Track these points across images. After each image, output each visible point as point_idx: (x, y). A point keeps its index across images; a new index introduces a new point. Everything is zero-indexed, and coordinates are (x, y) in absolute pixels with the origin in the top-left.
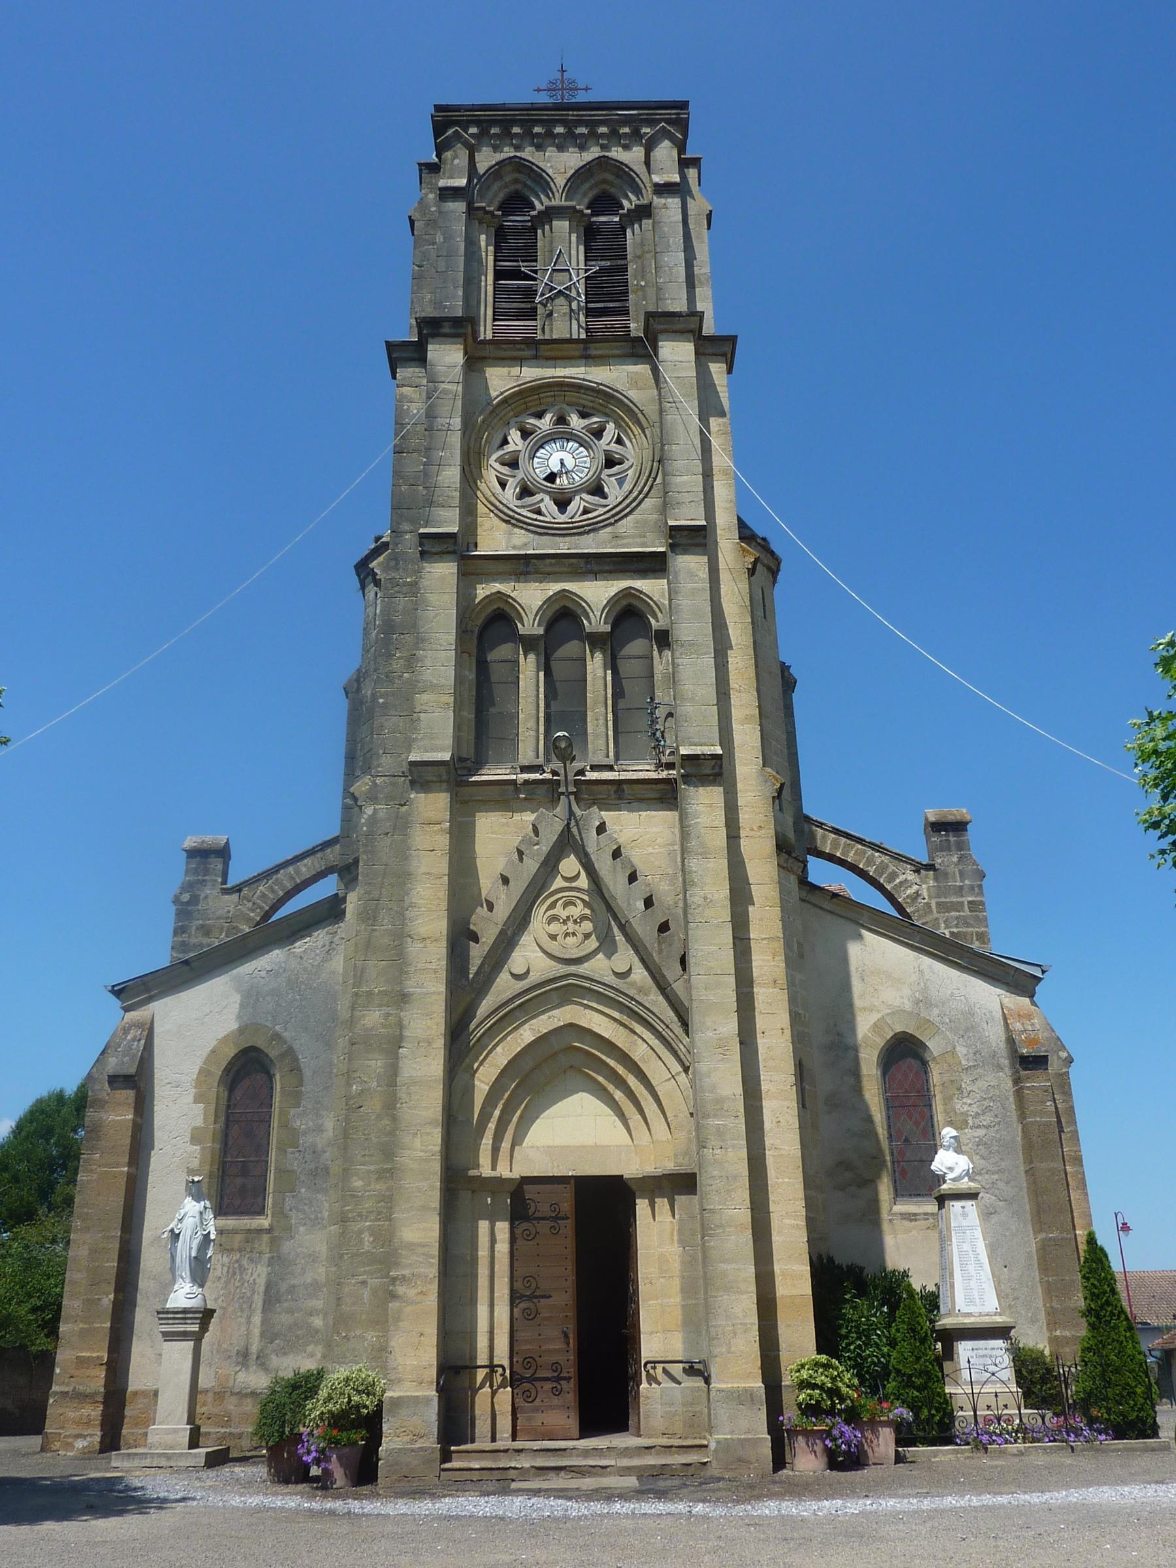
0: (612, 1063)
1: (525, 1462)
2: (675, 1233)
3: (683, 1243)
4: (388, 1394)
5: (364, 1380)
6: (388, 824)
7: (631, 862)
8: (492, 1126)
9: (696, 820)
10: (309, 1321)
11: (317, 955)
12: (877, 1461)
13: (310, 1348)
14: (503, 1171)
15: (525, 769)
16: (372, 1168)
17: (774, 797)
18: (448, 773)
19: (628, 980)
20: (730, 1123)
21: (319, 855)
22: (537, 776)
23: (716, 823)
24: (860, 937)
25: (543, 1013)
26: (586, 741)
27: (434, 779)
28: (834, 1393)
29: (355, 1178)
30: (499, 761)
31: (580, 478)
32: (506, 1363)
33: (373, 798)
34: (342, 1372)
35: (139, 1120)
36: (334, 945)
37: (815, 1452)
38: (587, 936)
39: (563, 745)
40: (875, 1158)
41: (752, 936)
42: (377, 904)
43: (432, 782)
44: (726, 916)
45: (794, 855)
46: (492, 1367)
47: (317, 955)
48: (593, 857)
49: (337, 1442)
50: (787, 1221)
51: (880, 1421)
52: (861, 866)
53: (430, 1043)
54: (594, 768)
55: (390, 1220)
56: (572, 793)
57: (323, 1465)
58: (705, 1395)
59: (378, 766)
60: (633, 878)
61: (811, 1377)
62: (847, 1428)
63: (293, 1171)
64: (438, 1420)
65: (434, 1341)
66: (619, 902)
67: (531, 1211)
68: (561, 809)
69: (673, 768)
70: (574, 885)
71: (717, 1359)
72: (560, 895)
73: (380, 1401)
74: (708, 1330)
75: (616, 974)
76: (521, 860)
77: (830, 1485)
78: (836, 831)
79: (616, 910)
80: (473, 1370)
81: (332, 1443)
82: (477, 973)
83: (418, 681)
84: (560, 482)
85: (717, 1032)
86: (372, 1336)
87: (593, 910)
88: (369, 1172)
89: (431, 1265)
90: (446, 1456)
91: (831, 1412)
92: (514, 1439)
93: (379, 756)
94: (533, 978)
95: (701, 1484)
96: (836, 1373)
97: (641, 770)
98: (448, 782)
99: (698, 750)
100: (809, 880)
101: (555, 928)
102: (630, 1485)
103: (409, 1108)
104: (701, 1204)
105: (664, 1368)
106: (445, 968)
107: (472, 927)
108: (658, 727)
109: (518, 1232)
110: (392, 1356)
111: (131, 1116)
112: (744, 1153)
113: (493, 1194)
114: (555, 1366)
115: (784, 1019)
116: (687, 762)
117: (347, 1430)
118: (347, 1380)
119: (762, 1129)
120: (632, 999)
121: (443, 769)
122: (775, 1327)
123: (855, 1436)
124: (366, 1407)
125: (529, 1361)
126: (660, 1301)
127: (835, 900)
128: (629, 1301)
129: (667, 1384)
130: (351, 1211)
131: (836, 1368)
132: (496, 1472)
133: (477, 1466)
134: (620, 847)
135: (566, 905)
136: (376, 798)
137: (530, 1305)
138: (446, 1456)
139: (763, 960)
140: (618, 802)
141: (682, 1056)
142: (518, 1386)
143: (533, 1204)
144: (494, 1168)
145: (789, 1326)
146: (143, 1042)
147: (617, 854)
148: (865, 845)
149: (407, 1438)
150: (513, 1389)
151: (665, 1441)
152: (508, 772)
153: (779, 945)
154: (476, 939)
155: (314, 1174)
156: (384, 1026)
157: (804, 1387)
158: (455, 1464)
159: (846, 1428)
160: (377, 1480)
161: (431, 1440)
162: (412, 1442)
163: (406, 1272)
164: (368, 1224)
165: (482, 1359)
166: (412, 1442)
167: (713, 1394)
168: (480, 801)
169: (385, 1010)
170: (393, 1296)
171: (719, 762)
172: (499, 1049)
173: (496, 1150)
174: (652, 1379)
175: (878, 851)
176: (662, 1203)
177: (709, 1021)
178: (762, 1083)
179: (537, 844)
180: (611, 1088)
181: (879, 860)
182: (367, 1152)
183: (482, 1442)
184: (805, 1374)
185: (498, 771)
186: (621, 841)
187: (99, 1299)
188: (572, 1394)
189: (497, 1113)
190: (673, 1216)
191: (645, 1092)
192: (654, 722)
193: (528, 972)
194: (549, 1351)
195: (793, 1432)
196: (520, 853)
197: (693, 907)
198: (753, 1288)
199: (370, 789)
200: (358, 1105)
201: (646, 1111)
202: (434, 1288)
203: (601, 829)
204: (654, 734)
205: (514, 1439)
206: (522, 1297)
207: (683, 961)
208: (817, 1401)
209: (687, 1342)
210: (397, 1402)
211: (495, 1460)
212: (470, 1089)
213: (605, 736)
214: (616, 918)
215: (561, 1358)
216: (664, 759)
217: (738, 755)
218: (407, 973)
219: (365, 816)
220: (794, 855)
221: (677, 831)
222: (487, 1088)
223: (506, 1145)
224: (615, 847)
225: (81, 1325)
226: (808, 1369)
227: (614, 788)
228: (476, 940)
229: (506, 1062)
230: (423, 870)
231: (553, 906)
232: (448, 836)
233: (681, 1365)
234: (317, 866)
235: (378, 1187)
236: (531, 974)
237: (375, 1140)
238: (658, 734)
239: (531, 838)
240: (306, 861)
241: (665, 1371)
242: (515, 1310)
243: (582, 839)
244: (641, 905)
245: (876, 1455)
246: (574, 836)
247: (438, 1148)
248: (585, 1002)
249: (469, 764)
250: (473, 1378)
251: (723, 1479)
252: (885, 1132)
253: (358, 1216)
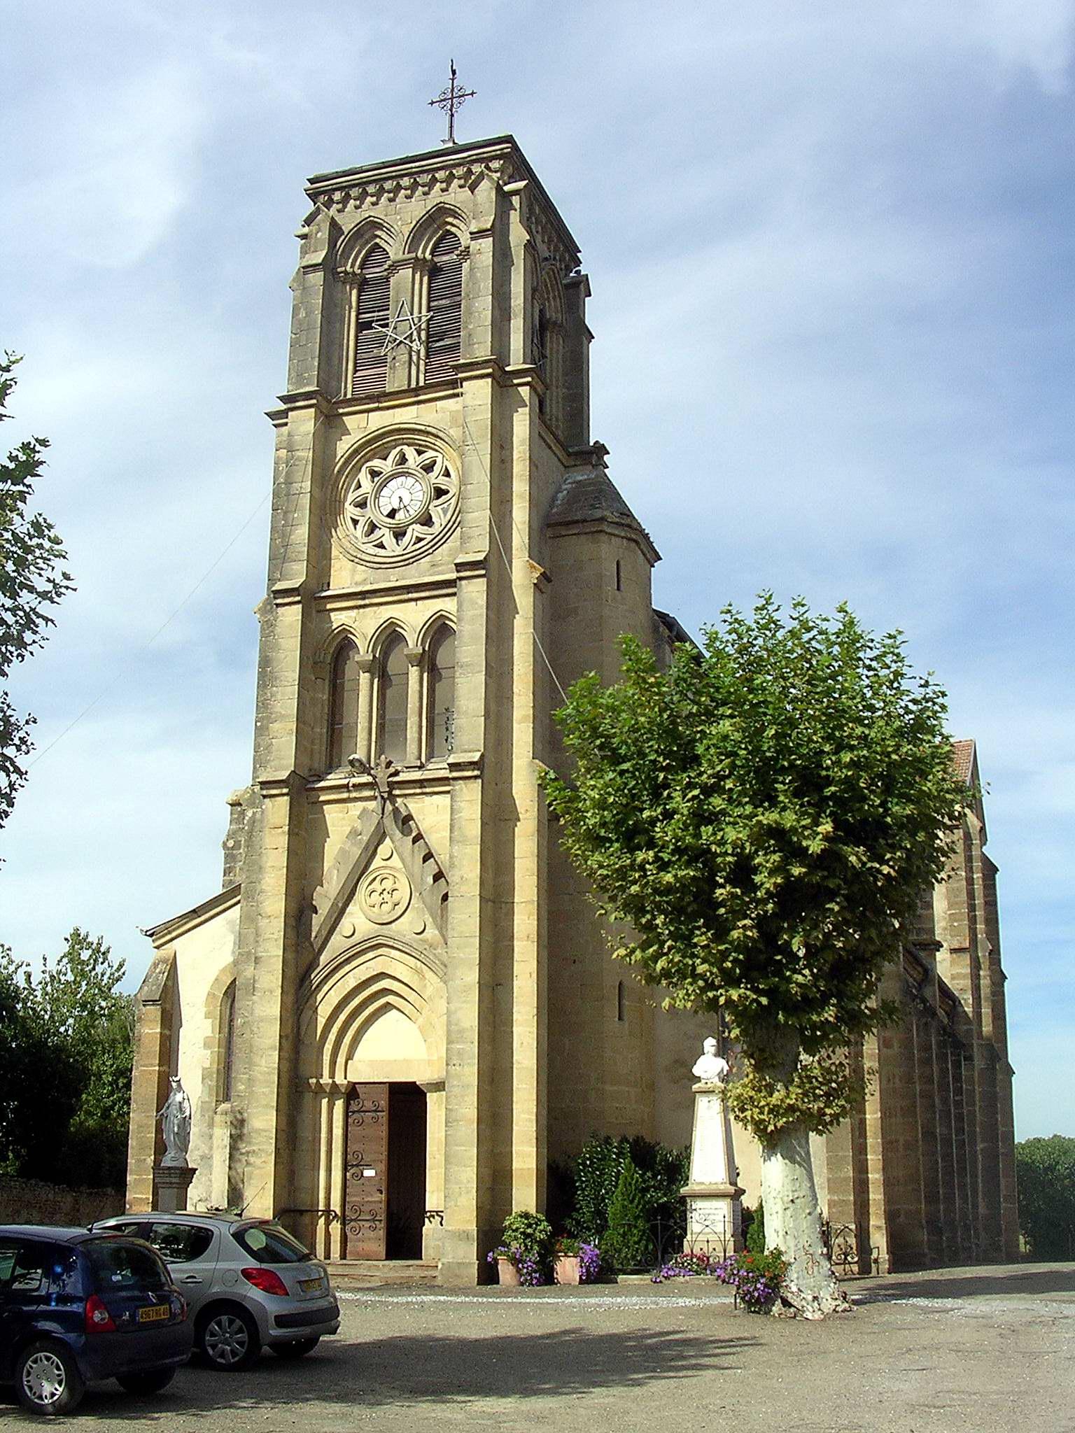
23: (474, 816)
31: (415, 510)
35: (167, 1032)
41: (516, 900)
50: (523, 1116)
53: (271, 992)
83: (271, 713)
84: (400, 516)
111: (159, 1030)
146: (166, 974)
165: (321, 1207)
177: (459, 973)
187: (145, 1160)
225: (135, 1177)
242: (348, 1174)
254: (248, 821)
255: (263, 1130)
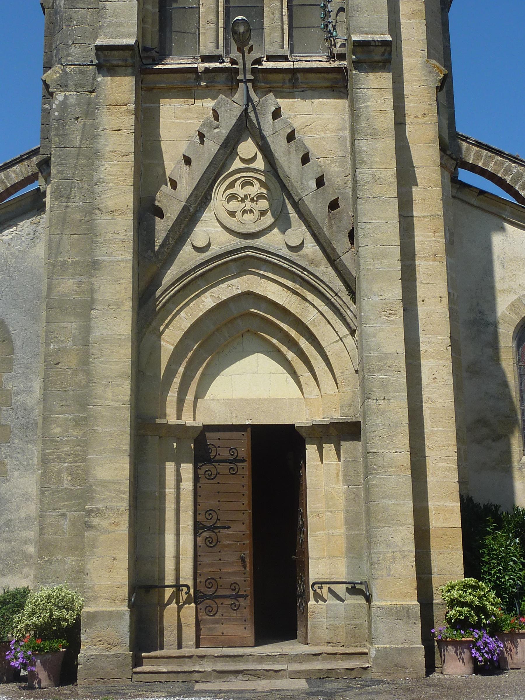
0: (285, 327)
1: (207, 667)
2: (341, 473)
3: (347, 482)
4: (86, 609)
5: (64, 597)
6: (78, 109)
7: (304, 144)
8: (177, 381)
9: (365, 104)
10: (24, 548)
11: (22, 242)
12: (515, 666)
13: (26, 570)
14: (187, 420)
15: (205, 59)
16: (69, 416)
17: (437, 87)
18: (133, 57)
19: (301, 253)
20: (392, 377)
21: (26, 163)
22: (218, 65)
24: (503, 229)
25: (223, 282)
26: (262, 35)
27: (120, 63)
28: (481, 610)
29: (54, 426)
30: (182, 53)
32: (190, 583)
33: (63, 86)
34: (45, 591)
36: (37, 234)
37: (463, 659)
38: (263, 213)
39: (242, 29)
40: (508, 417)
41: (415, 214)
42: (72, 183)
43: (118, 66)
44: (393, 192)
45: (449, 152)
46: (178, 587)
47: (22, 242)
48: (269, 140)
49: (41, 650)
50: (440, 464)
51: (519, 633)
52: (500, 175)
53: (118, 306)
54: (270, 58)
55: (85, 461)
56: (250, 81)
57: (29, 668)
58: (365, 611)
59: (68, 55)
60: (305, 159)
61: (460, 596)
62: (491, 639)
63: (7, 425)
64: (130, 631)
65: (126, 564)
66: (293, 181)
67: (212, 455)
68: (239, 96)
69: (344, 59)
70: (251, 166)
71: (379, 581)
72: (238, 176)
73: (79, 615)
74: (369, 557)
75: (291, 248)
76: (202, 142)
77: (480, 689)
78: (479, 145)
79: (290, 189)
80: (162, 589)
81: (37, 650)
82: (162, 246)
85: (383, 297)
86: (71, 560)
87: (268, 190)
88: (66, 420)
89: (123, 499)
90: (137, 661)
91: (478, 626)
92: (198, 646)
93: (68, 47)
94: (213, 251)
95: (363, 686)
96: (483, 593)
97: (314, 61)
98: (133, 66)
99: (369, 38)
100: (459, 178)
101: (234, 205)
102: (301, 687)
103: (101, 363)
104: (365, 447)
105: (329, 588)
106: (131, 238)
107: (157, 204)
108: (330, 20)
109: (201, 472)
110: (88, 578)
112: (405, 404)
113: (179, 440)
114: (234, 586)
115: (442, 289)
116: (359, 49)
117: (49, 639)
118: (49, 598)
119: (420, 384)
120: (304, 269)
121: (127, 54)
122: (428, 555)
123: (498, 647)
124: (66, 620)
125: (211, 582)
126: (326, 532)
127: (481, 196)
128: (298, 532)
129: (332, 601)
130: (50, 454)
131: (483, 589)
132: (181, 675)
133: (165, 670)
134: (293, 131)
135: (244, 185)
136: (66, 86)
137: (212, 534)
138: (137, 661)
139: (425, 236)
140: (291, 90)
141: (349, 321)
142: (201, 602)
143: (214, 449)
144: (179, 417)
145: (440, 553)
147: (291, 137)
148: (503, 157)
149: (102, 647)
150: (196, 604)
151: (329, 649)
152: (190, 61)
153: (440, 223)
154: (161, 215)
155: (25, 427)
156: (77, 292)
157: (455, 605)
158: (146, 668)
159: (490, 640)
160: (76, 680)
161: (124, 648)
162: (107, 649)
163: (100, 506)
164: (66, 465)
165: (169, 579)
166: (107, 649)
167: (373, 610)
168: (164, 88)
169: (78, 278)
170: (89, 526)
171: (388, 49)
172: (182, 314)
173: (180, 402)
174: (318, 597)
175: (515, 162)
176: (329, 448)
178: (421, 344)
179: (217, 127)
180: (284, 349)
181: (515, 170)
182: (64, 404)
183: (171, 650)
184: (455, 594)
185: (181, 61)
186: (295, 126)
188: (248, 609)
189: (181, 370)
190: (339, 459)
191: (315, 353)
192: (326, 14)
193: (209, 245)
194: (228, 573)
195: (443, 643)
196: (201, 136)
197: (362, 184)
198: (411, 520)
199: (61, 77)
200: (55, 362)
201: (316, 369)
202: (125, 519)
203: (276, 114)
204: (327, 26)
205: (198, 646)
206: (204, 527)
207: (351, 236)
208: (466, 617)
209: (351, 566)
210: (94, 617)
211: (181, 665)
212: (157, 349)
213: (280, 30)
214: (290, 196)
215: (239, 579)
216: (336, 50)
217: (405, 47)
218: (96, 242)
219: (57, 102)
220: (449, 152)
221: (347, 117)
222: (172, 348)
223: (190, 398)
224: (289, 131)
226: (458, 590)
227: (289, 76)
228: (162, 216)
229: (189, 325)
230: (110, 148)
231: (232, 185)
232: (134, 116)
233: (345, 586)
234: (25, 172)
235: (74, 433)
236: (212, 247)
237: (71, 392)
238: (330, 27)
239: (211, 122)
240: (15, 168)
241: (330, 590)
242: (198, 539)
243: (259, 123)
244: (313, 184)
245: (514, 661)
246: (251, 120)
247: (128, 398)
248: (261, 272)
249: (153, 53)
250: (162, 595)
251: (383, 681)
252: (518, 395)
253: (58, 458)
254: (57, 105)
255: (109, 482)
